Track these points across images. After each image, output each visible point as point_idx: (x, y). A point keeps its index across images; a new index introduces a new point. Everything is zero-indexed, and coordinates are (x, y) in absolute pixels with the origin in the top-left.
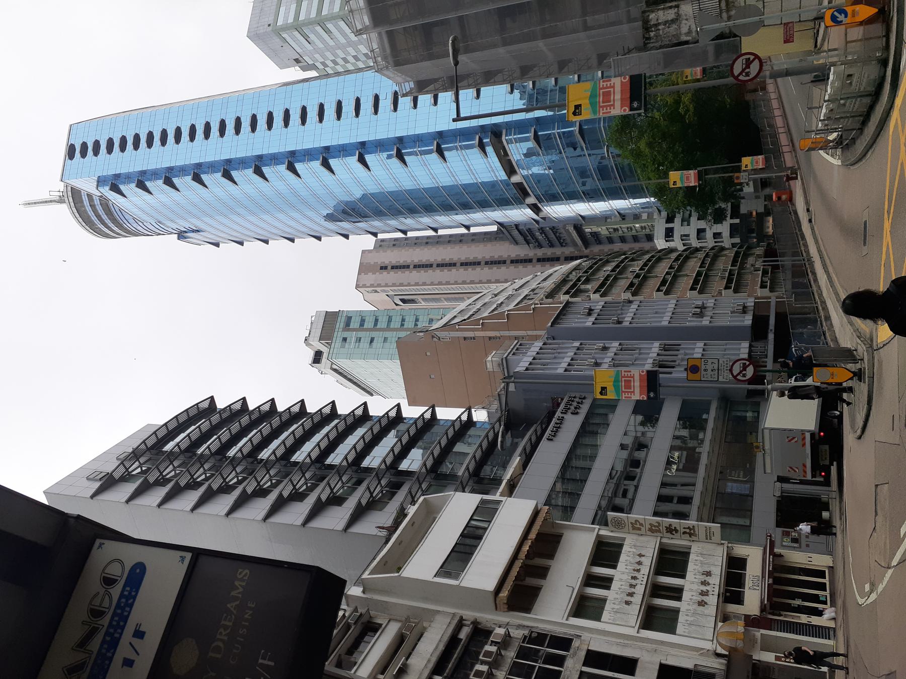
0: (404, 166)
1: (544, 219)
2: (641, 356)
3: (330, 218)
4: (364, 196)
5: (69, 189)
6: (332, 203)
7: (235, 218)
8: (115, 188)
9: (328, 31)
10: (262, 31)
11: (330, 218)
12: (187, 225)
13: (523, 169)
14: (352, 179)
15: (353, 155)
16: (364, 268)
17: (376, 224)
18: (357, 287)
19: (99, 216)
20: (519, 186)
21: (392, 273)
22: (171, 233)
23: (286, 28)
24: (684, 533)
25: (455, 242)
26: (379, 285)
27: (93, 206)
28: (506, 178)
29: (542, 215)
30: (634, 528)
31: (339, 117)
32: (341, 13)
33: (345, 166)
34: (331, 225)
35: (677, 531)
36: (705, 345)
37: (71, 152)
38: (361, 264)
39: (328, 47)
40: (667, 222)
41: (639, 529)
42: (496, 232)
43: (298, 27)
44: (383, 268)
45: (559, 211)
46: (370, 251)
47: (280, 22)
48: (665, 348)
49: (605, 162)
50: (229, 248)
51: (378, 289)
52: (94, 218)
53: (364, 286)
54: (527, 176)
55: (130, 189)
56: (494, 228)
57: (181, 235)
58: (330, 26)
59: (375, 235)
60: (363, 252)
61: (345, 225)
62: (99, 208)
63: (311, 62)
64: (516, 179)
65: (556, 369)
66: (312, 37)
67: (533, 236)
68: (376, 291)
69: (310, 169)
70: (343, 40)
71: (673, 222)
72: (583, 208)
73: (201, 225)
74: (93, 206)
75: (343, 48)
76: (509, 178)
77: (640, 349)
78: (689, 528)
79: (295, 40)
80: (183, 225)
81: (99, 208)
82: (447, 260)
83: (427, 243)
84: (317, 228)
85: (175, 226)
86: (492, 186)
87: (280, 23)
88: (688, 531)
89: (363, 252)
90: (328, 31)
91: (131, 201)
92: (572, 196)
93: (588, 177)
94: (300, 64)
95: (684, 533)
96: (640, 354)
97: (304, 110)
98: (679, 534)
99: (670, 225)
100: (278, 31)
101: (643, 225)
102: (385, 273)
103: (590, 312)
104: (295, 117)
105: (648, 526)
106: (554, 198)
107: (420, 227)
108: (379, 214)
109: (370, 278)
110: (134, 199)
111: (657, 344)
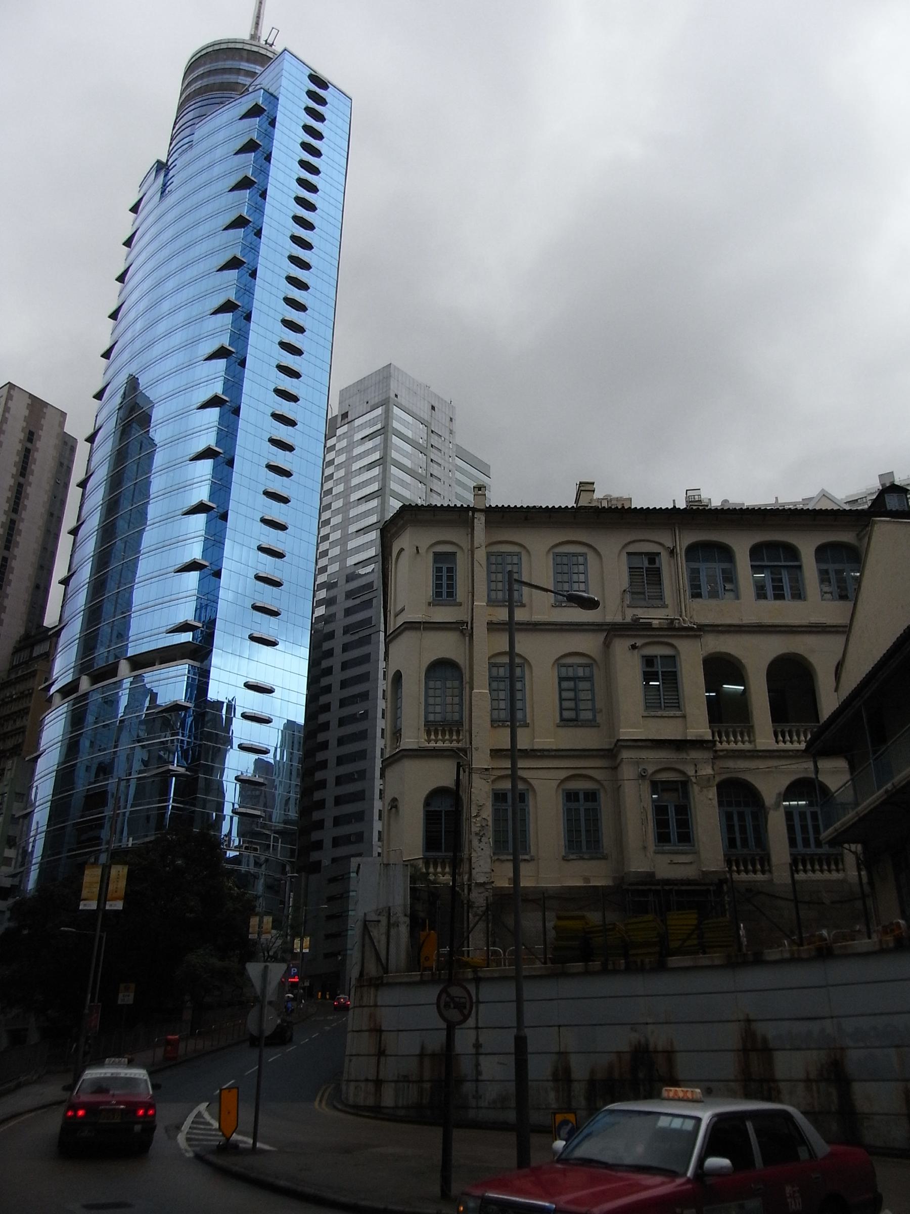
1: (50, 700)
3: (133, 383)
4: (152, 443)
5: (270, 55)
6: (152, 394)
8: (255, 111)
11: (133, 383)
12: (176, 181)
13: (131, 683)
15: (218, 443)
16: (37, 406)
17: (105, 448)
19: (222, 75)
20: (111, 671)
21: (19, 447)
23: (387, 415)
29: (57, 699)
31: (273, 441)
33: (205, 428)
34: (122, 379)
38: (45, 404)
39: (351, 459)
42: (40, 625)
43: (385, 431)
44: (31, 437)
45: (54, 728)
46: (62, 424)
47: (396, 410)
50: (126, 223)
53: (9, 397)
54: (120, 687)
56: (50, 619)
57: (161, 167)
58: (376, 471)
59: (91, 439)
60: (64, 415)
62: (232, 78)
63: (339, 432)
66: (369, 444)
67: (19, 680)
69: (212, 379)
70: (355, 481)
72: (48, 763)
73: (170, 200)
74: (230, 71)
75: (346, 479)
76: (129, 659)
79: (367, 422)
80: (177, 177)
83: (52, 515)
87: (396, 410)
89: (64, 415)
92: (72, 747)
93: (97, 775)
94: (339, 419)
97: (293, 398)
100: (385, 403)
102: (21, 436)
104: (287, 384)
106: (76, 720)
107: (83, 507)
108: (120, 457)
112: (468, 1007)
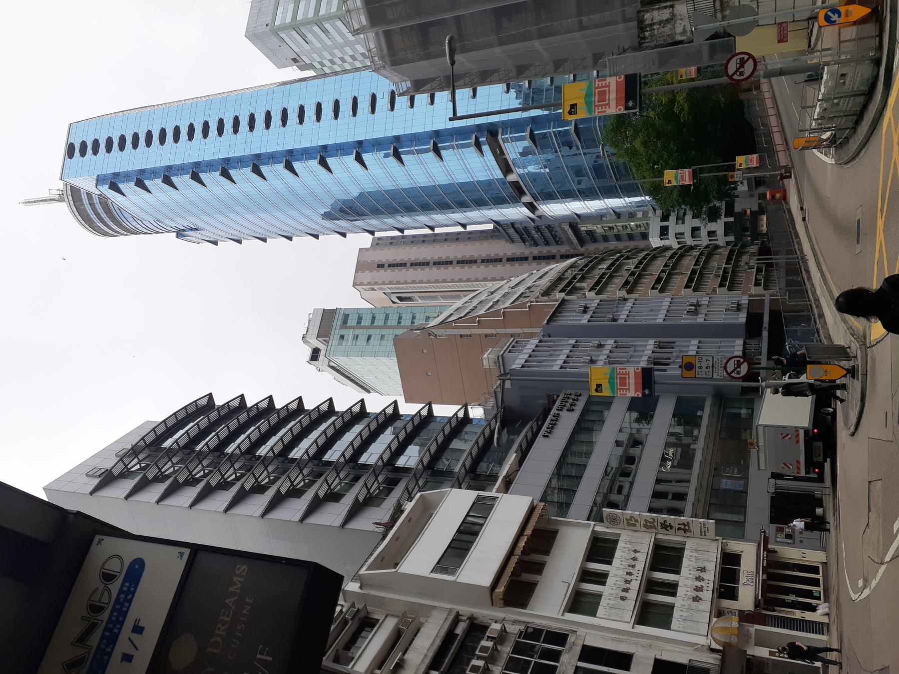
0: (401, 165)
1: (540, 217)
2: (636, 353)
3: (327, 216)
4: (361, 195)
5: (69, 187)
6: (330, 202)
7: (233, 216)
8: (114, 187)
9: (325, 31)
10: (260, 31)
11: (327, 216)
12: (186, 224)
13: (519, 167)
14: (349, 178)
15: (350, 154)
16: (361, 266)
17: (373, 222)
18: (355, 284)
19: (98, 214)
20: (515, 185)
21: (389, 271)
22: (170, 231)
23: (284, 28)
24: (679, 529)
25: (451, 241)
26: (376, 283)
27: (92, 205)
28: (502, 176)
29: (537, 213)
30: (629, 524)
31: (336, 116)
32: (339, 13)
33: (342, 165)
34: (328, 224)
35: (671, 527)
36: (699, 342)
37: (70, 151)
38: (358, 262)
39: (325, 47)
40: (662, 221)
41: (634, 525)
42: (493, 231)
43: (295, 26)
44: (380, 266)
45: (555, 209)
46: (367, 249)
47: (278, 22)
48: (660, 346)
49: (600, 161)
50: (227, 246)
51: (375, 287)
52: (93, 217)
53: (361, 284)
54: (523, 175)
55: (129, 187)
56: (490, 226)
57: (180, 234)
58: (327, 26)
59: (372, 233)
60: (361, 250)
61: (343, 224)
62: (98, 207)
63: (308, 62)
64: (512, 178)
65: (552, 366)
66: (310, 37)
67: (529, 234)
68: (373, 289)
69: (308, 168)
70: (340, 40)
71: (668, 220)
72: (578, 207)
73: (199, 224)
74: (92, 205)
75: (340, 47)
76: (505, 176)
77: (635, 346)
78: (683, 524)
79: (293, 40)
80: (182, 223)
81: (98, 207)
82: (444, 258)
83: (424, 241)
84: (314, 226)
85: (173, 225)
86: (488, 184)
87: (278, 23)
88: (682, 527)
89: (361, 250)
90: (325, 31)
91: (130, 200)
92: (567, 195)
93: (583, 175)
94: (298, 64)
95: (679, 529)
96: (635, 351)
97: (302, 109)
98: (673, 530)
99: (665, 224)
100: (276, 31)
101: (638, 223)
102: (382, 271)
103: (585, 310)
104: (293, 116)
105: (643, 522)
106: (549, 197)
107: (417, 225)
108: (376, 212)
109: (367, 276)
110: (133, 197)
111: (651, 342)
112: (742, 56)
